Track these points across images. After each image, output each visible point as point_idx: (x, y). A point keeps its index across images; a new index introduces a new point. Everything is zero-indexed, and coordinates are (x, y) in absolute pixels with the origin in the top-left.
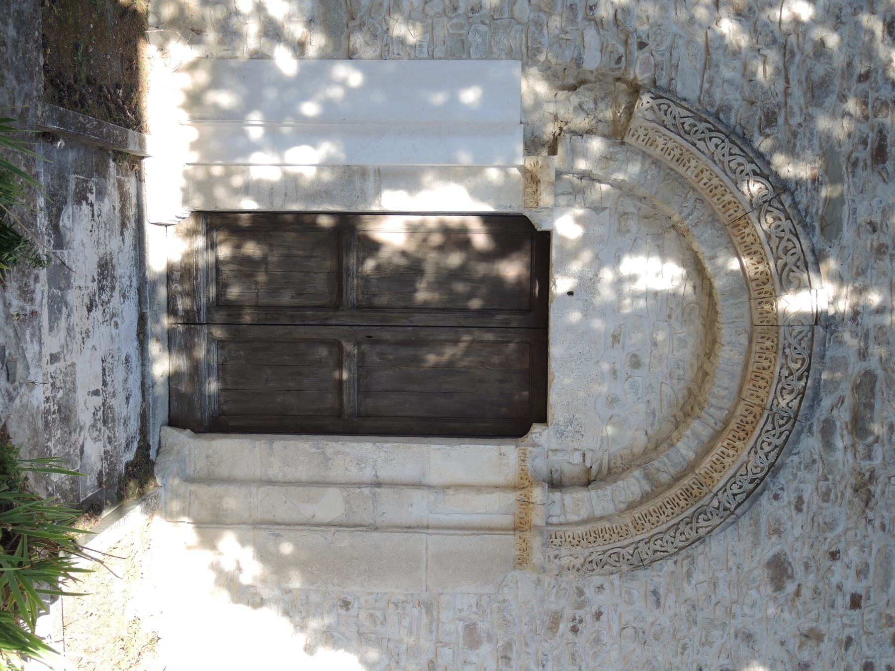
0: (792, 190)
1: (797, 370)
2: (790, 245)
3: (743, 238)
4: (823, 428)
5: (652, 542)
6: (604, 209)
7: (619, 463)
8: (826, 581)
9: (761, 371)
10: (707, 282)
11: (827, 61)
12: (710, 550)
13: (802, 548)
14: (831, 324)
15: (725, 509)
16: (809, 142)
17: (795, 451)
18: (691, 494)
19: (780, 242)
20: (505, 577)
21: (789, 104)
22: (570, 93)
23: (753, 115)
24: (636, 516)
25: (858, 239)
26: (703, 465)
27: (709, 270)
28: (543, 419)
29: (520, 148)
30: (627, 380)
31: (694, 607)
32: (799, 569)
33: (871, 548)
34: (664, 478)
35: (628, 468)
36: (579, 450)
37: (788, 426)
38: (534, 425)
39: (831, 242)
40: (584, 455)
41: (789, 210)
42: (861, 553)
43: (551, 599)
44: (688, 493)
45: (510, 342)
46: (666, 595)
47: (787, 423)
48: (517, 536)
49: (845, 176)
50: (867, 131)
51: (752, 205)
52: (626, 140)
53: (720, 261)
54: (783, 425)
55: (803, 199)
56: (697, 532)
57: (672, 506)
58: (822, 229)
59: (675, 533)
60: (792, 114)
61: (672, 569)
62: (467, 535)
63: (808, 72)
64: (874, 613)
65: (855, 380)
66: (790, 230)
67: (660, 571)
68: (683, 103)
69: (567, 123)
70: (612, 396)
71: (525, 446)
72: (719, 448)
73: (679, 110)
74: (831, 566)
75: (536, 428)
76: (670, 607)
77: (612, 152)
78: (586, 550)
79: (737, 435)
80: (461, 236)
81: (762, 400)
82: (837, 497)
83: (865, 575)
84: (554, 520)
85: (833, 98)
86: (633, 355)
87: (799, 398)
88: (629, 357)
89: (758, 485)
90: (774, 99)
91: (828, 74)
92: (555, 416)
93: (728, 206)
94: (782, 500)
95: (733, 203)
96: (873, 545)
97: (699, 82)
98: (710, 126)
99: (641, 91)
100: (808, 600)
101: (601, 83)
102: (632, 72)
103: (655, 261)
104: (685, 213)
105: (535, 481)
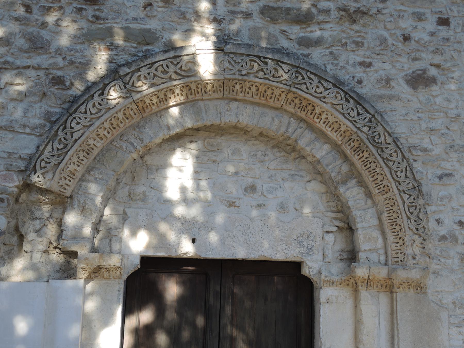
0: (116, 66)
1: (259, 65)
2: (160, 69)
3: (153, 104)
4: (305, 46)
5: (399, 179)
6: (125, 213)
7: (334, 204)
8: (427, 44)
9: (259, 92)
10: (187, 132)
11: (13, 37)
12: (404, 133)
13: (401, 62)
14: (223, 39)
15: (370, 121)
16: (78, 52)
17: (323, 68)
18: (358, 148)
19: (157, 76)
20: (433, 302)
21: (47, 66)
22: (25, 240)
23: (54, 95)
24: (377, 191)
25: (157, 17)
26: (335, 138)
27: (178, 131)
28: (298, 265)
29: (69, 283)
30: (265, 196)
31: (451, 147)
32: (418, 65)
33: (400, 10)
34: (345, 168)
35: (338, 197)
36: (323, 236)
37: (303, 73)
38: (303, 272)
39: (159, 37)
40: (327, 232)
41: (132, 69)
42: (405, 18)
43: (450, 263)
44: (358, 150)
45: (233, 291)
46: (442, 168)
47: (301, 74)
48: (398, 290)
49: (106, 25)
50: (71, 8)
51: (127, 97)
52: (68, 194)
53: (171, 122)
54: (303, 76)
55: (123, 58)
56: (389, 144)
57: (368, 163)
58: (148, 44)
59: (391, 161)
60: (55, 64)
61: (420, 163)
62: (398, 334)
63: (21, 51)
64: (452, 8)
65: (267, 21)
66: (148, 68)
67: (422, 173)
68: (41, 148)
69: (51, 243)
70: (279, 207)
71: (320, 282)
72: (321, 126)
73: (46, 152)
74: (415, 41)
75: (305, 271)
76: (452, 166)
77: (78, 206)
78: (407, 233)
79: (310, 112)
80: (141, 333)
81: (283, 92)
82: (360, 36)
83: (421, 15)
84: (382, 258)
85: (44, 33)
86: (245, 191)
87: (281, 64)
88: (247, 194)
89: (350, 96)
90: (42, 77)
91: (24, 36)
92: (295, 255)
93: (128, 115)
94: (362, 78)
95: (125, 112)
96: (398, 9)
97: (24, 136)
98: (61, 128)
99: (29, 182)
100: (443, 58)
101: (19, 214)
102: (12, 189)
103: (171, 173)
104: (132, 149)
105: (350, 273)
